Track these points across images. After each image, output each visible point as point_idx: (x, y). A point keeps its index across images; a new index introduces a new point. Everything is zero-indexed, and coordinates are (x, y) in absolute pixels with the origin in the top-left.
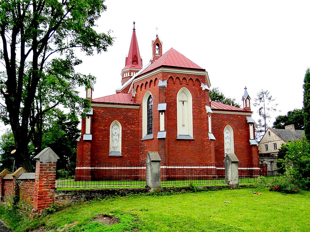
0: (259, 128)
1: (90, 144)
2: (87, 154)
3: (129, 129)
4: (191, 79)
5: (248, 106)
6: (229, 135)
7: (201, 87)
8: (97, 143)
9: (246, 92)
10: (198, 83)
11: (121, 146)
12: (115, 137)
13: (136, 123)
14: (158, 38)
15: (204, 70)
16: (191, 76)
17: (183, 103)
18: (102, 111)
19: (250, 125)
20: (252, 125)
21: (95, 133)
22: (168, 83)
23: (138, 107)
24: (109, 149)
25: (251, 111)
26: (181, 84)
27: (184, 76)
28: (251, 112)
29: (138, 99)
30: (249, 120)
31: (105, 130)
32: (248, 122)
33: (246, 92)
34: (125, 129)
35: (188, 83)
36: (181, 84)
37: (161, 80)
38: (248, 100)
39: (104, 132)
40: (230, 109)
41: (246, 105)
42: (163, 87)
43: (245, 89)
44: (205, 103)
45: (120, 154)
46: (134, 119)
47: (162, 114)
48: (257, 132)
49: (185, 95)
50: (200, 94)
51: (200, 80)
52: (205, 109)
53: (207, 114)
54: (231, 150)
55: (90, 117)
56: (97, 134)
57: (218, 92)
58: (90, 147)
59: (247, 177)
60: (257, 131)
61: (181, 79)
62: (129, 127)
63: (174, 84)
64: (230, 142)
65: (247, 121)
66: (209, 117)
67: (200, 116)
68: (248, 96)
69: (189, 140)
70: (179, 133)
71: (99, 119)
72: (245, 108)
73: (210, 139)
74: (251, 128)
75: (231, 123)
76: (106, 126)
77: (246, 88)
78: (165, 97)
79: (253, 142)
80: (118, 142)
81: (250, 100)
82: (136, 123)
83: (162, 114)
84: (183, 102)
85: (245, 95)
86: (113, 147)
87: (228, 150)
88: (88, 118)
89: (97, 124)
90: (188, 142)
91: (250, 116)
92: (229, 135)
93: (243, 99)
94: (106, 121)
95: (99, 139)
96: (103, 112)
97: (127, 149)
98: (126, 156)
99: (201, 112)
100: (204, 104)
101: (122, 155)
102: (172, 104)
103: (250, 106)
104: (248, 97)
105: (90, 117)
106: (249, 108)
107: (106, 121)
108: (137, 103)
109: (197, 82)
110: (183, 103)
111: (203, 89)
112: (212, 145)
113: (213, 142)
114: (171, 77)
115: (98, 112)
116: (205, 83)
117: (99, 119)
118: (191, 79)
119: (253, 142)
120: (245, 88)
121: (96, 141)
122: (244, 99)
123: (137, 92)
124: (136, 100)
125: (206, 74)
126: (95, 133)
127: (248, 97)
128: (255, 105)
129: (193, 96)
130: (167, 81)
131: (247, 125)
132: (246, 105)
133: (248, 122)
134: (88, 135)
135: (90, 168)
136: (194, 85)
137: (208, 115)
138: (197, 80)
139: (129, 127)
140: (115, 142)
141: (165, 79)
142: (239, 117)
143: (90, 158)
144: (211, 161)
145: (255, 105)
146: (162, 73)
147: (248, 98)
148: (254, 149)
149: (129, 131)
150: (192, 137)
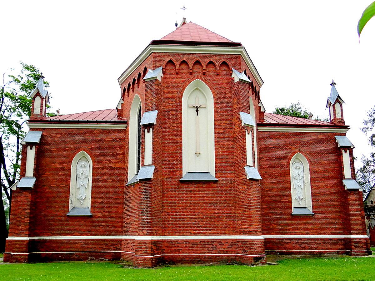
0: (372, 166)
1: (30, 195)
2: (23, 213)
3: (106, 166)
4: (211, 63)
5: (339, 116)
6: (300, 172)
7: (232, 76)
8: (46, 193)
9: (334, 91)
10: (227, 69)
11: (91, 197)
12: (80, 182)
13: (119, 154)
14: (184, 22)
15: (239, 45)
16: (211, 57)
17: (197, 111)
18: (59, 136)
19: (343, 151)
20: (348, 151)
21: (45, 176)
22: (164, 73)
23: (122, 126)
24: (69, 202)
25: (346, 125)
26: (191, 74)
27: (197, 59)
28: (347, 127)
29: (125, 113)
30: (341, 142)
31: (63, 169)
32: (339, 146)
33: (334, 91)
34: (98, 166)
35: (205, 71)
36: (191, 74)
37: (151, 69)
38: (337, 105)
39: (60, 173)
40: (302, 123)
41: (335, 115)
42: (154, 80)
43: (331, 85)
44: (239, 106)
45: (88, 212)
46: (115, 148)
47: (148, 132)
48: (370, 172)
49: (200, 96)
50: (230, 91)
51: (230, 63)
52: (239, 118)
53: (244, 127)
54: (307, 201)
55: (34, 148)
56: (47, 176)
57: (299, 110)
58: (30, 200)
59: (338, 253)
60: (370, 171)
61: (191, 65)
62: (106, 161)
63: (177, 74)
64: (304, 185)
65: (337, 144)
66: (249, 133)
67: (229, 135)
68: (339, 96)
69: (208, 183)
70: (186, 169)
71: (53, 149)
72: (333, 120)
73: (248, 178)
74: (346, 157)
75: (305, 149)
76: (64, 162)
77: (333, 84)
78: (156, 98)
79: (349, 184)
80: (87, 189)
81: (343, 105)
82: (119, 154)
83: (148, 132)
84: (197, 109)
85: (332, 96)
86: (77, 199)
87: (300, 199)
88: (31, 149)
89: (47, 159)
90: (204, 186)
91: (344, 134)
92: (300, 172)
93: (329, 104)
94: (65, 153)
95: (52, 185)
96: (60, 138)
97: (102, 202)
98: (99, 215)
99: (232, 125)
100: (237, 110)
101: (91, 214)
102: (173, 113)
103: (342, 116)
104: (338, 98)
105: (34, 148)
106: (342, 120)
107: (65, 153)
108: (125, 119)
109: (223, 68)
110: (197, 111)
111: (236, 80)
112: (254, 191)
113: (255, 185)
114: (171, 62)
115: (52, 138)
116: (239, 69)
117: (53, 149)
118: (211, 63)
119: (349, 184)
120: (331, 82)
121: (46, 189)
122: (331, 103)
123: (124, 101)
124: (122, 116)
125: (241, 52)
126: (45, 176)
127: (338, 98)
128: (364, 130)
129: (215, 97)
130: (162, 69)
131: (338, 151)
132: (335, 115)
133: (339, 146)
134: (29, 179)
135: (26, 238)
136: (218, 74)
137: (244, 130)
138: (224, 63)
139: (106, 161)
140: (82, 189)
141: (158, 64)
142: (321, 137)
143: (28, 220)
144: (250, 225)
145: (364, 130)
146: (152, 55)
147: (339, 100)
148: (352, 198)
149: (105, 170)
150: (213, 176)
